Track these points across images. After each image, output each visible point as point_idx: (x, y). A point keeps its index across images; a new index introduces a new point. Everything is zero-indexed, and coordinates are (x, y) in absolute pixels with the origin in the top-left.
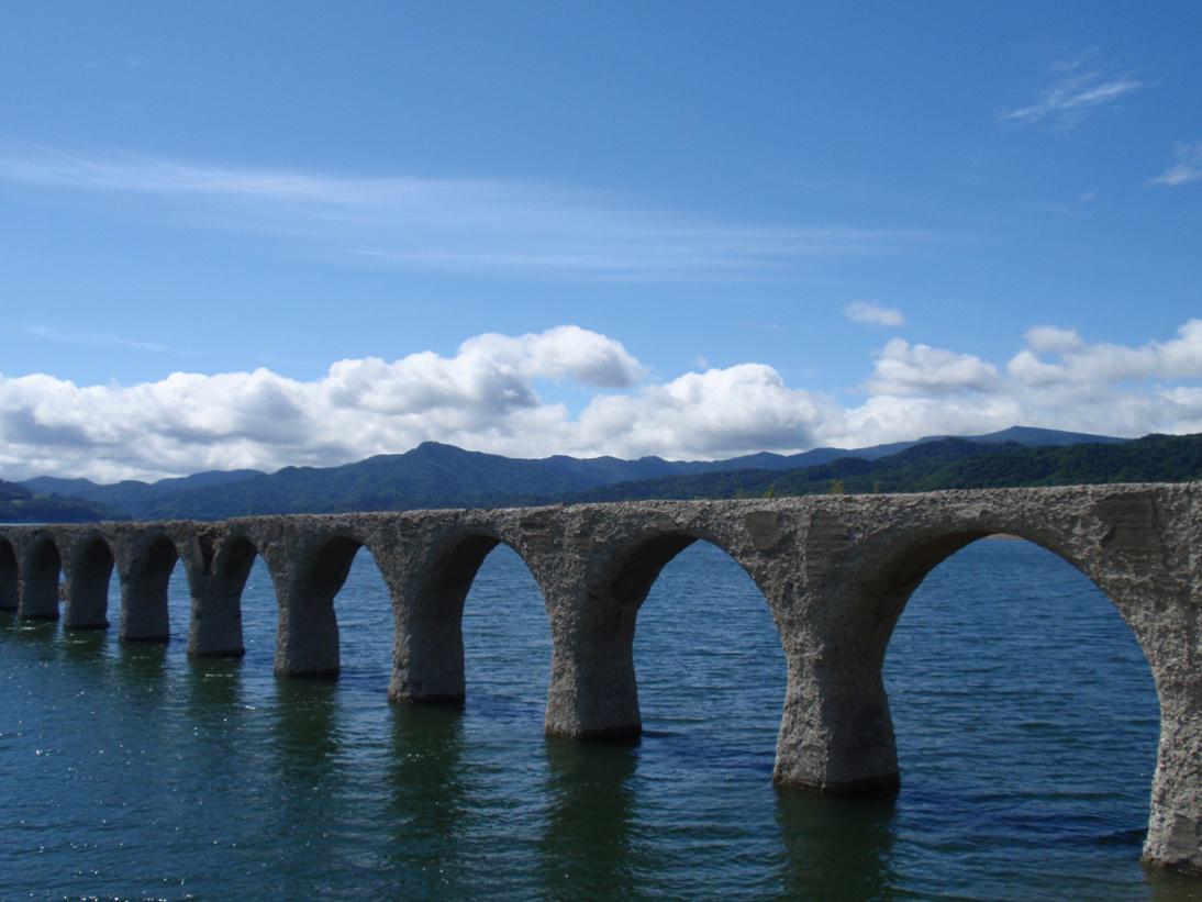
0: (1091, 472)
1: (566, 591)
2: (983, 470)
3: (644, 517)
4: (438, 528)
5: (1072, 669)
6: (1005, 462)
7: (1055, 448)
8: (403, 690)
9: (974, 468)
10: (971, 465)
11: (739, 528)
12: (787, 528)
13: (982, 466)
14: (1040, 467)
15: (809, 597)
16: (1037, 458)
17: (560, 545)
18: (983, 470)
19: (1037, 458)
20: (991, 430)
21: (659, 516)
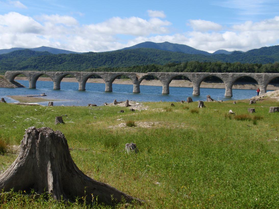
0: (76, 63)
1: (229, 82)
2: (42, 60)
3: (242, 74)
4: (205, 75)
5: (88, 128)
6: (49, 58)
7: (65, 55)
8: (197, 94)
9: (40, 60)
10: (39, 59)
11: (255, 76)
12: (261, 76)
13: (42, 59)
14: (60, 60)
15: (264, 82)
16: (60, 57)
17: (228, 77)
18: (42, 60)
19: (60, 57)
20: (30, 48)
21: (244, 74)
